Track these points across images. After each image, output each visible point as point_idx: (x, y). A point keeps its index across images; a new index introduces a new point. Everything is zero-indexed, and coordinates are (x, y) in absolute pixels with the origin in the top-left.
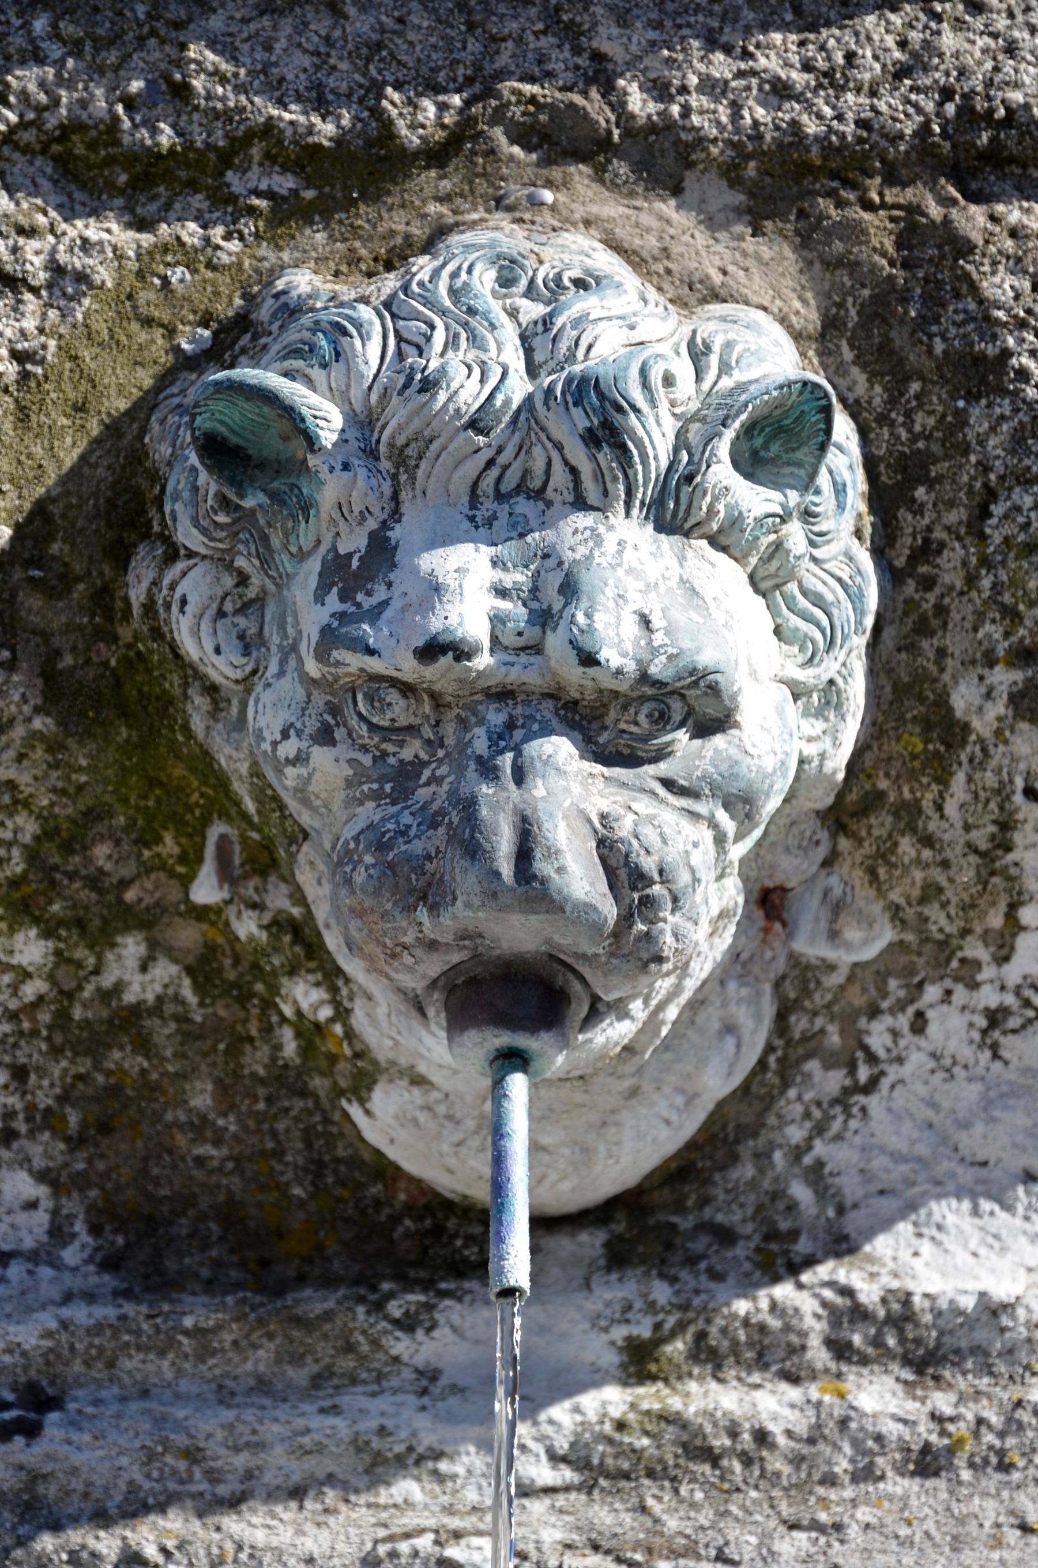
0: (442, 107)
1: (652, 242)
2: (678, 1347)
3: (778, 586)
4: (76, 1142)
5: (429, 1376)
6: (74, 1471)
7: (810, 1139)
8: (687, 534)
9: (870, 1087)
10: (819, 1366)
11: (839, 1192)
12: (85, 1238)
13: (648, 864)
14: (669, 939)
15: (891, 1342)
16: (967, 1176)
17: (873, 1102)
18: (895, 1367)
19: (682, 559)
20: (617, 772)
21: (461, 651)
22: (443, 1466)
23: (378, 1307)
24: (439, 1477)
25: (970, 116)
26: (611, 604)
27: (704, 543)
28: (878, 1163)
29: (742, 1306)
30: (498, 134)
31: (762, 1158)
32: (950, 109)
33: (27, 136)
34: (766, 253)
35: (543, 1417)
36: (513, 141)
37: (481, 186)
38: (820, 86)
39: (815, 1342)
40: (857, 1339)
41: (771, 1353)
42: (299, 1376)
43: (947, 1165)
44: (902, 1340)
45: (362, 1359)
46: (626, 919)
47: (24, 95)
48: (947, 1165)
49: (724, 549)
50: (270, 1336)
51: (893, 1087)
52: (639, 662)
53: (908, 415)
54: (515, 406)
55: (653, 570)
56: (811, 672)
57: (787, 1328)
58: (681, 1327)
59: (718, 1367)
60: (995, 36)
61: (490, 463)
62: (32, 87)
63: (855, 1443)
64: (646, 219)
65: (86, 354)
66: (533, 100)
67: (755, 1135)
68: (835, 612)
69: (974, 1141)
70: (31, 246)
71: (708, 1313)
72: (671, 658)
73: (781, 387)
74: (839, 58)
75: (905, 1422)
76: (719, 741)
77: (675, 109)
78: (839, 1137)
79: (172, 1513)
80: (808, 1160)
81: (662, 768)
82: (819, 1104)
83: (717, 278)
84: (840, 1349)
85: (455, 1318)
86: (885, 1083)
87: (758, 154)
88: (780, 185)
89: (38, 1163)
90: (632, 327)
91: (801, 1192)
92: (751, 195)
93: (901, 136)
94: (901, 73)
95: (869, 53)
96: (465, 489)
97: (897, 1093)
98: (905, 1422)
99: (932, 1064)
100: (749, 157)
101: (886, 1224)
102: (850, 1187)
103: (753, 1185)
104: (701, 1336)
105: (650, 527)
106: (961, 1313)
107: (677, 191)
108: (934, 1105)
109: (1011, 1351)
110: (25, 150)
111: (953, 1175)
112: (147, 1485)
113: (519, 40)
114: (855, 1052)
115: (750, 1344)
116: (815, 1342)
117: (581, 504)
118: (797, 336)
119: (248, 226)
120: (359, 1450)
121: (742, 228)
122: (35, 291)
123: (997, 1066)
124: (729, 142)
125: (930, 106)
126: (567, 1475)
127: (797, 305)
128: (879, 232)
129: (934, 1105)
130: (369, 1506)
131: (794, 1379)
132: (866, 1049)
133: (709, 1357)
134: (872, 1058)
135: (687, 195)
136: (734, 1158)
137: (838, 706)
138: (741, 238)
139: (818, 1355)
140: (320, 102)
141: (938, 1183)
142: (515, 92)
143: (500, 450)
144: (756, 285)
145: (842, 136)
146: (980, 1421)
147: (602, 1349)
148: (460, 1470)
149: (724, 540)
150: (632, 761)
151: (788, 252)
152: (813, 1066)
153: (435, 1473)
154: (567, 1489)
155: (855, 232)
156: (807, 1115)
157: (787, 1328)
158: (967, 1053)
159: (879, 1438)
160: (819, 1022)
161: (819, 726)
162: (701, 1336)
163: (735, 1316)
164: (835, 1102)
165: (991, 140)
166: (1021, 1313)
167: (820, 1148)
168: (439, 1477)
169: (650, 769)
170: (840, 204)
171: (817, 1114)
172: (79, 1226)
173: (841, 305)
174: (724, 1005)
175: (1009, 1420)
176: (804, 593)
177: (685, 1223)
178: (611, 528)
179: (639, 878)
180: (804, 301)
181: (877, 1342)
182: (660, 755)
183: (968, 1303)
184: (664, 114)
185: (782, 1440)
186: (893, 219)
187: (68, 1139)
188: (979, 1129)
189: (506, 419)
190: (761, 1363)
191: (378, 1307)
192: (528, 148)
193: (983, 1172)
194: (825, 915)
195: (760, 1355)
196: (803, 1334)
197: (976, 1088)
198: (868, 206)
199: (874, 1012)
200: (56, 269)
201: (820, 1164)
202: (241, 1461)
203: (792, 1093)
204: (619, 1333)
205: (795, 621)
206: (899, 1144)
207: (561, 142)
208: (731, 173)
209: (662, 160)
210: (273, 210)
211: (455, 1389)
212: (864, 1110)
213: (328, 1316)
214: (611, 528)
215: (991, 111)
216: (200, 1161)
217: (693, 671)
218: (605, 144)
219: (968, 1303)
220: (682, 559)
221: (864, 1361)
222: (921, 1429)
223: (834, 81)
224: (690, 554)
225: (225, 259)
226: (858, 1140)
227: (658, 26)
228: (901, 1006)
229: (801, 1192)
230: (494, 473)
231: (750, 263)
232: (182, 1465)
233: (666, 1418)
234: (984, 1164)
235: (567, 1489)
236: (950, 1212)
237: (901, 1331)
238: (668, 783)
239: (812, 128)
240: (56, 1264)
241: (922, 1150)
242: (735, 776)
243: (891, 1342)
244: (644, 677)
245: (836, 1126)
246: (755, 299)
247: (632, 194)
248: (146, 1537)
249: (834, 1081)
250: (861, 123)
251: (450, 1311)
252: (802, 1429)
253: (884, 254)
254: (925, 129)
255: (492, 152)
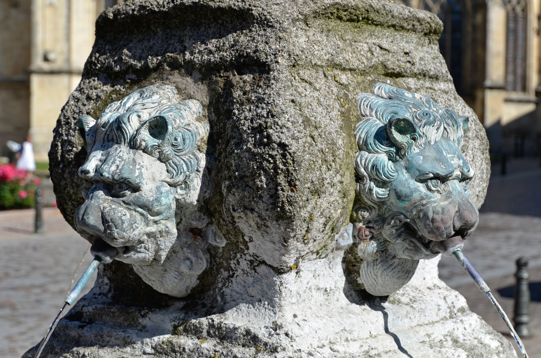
0: (157, 59)
1: (184, 86)
2: (181, 328)
3: (167, 161)
4: (114, 273)
5: (144, 327)
6: (85, 336)
7: (222, 287)
8: (137, 149)
9: (232, 276)
10: (204, 336)
11: (226, 299)
12: (113, 292)
13: (109, 218)
14: (116, 234)
15: (217, 333)
16: (249, 299)
17: (233, 279)
18: (217, 339)
19: (135, 154)
20: (115, 199)
21: (88, 172)
22: (135, 346)
23: (140, 312)
24: (133, 348)
25: (240, 56)
26: (110, 164)
27: (141, 151)
28: (234, 293)
29: (193, 321)
30: (165, 64)
31: (214, 289)
32: (237, 54)
33: (102, 69)
34: (202, 88)
35: (152, 338)
36: (167, 66)
37: (161, 76)
38: (217, 51)
39: (205, 331)
40: (211, 331)
41: (196, 332)
42: (126, 324)
43: (245, 296)
44: (219, 333)
45: (135, 322)
46: (105, 230)
47: (101, 61)
48: (245, 296)
49: (146, 153)
50: (123, 315)
51: (237, 277)
52: (112, 176)
53: (219, 124)
54: (110, 122)
55: (126, 157)
56: (172, 180)
57: (200, 327)
58: (182, 324)
59: (188, 334)
60: (251, 37)
61: (105, 134)
62: (102, 60)
63: (199, 354)
64: (184, 81)
65: (98, 112)
66: (171, 57)
67: (214, 285)
68: (179, 167)
69: (251, 290)
70: (94, 91)
71: (187, 321)
72: (119, 175)
73: (154, 118)
74: (222, 44)
75: (208, 350)
76: (137, 194)
77: (192, 57)
78: (227, 287)
79: (95, 347)
80: (222, 291)
81: (124, 199)
82: (224, 279)
83: (192, 93)
84: (209, 333)
85: (150, 316)
86: (235, 275)
87: (204, 66)
88: (206, 72)
89: (108, 276)
90: (144, 105)
91: (219, 298)
92: (203, 75)
93: (227, 61)
94: (233, 46)
95: (227, 43)
96: (102, 139)
97: (238, 278)
98: (208, 350)
99: (242, 272)
100: (203, 67)
101: (231, 308)
102: (228, 298)
103: (212, 295)
104: (186, 326)
105: (128, 148)
106: (230, 329)
107: (191, 75)
108: (245, 282)
109: (236, 339)
110: (102, 72)
111: (246, 298)
112: (94, 341)
113: (173, 44)
114: (229, 269)
115: (194, 330)
116: (205, 331)
117: (117, 143)
118: (203, 106)
119: (127, 86)
120: (124, 340)
121: (200, 83)
122: (93, 100)
123: (256, 274)
124: (199, 64)
125: (234, 54)
126: (153, 351)
127: (205, 99)
128: (221, 82)
129: (245, 282)
130: (122, 351)
131: (199, 338)
132: (231, 267)
133: (187, 331)
134: (232, 270)
135: (193, 76)
136: (210, 289)
137: (189, 188)
138: (199, 85)
139: (205, 334)
140: (139, 61)
141: (243, 300)
142: (168, 56)
143: (107, 131)
144: (198, 95)
145: (216, 61)
146: (222, 353)
147: (170, 327)
148: (137, 347)
149: (146, 151)
150: (118, 196)
151: (206, 88)
152: (222, 270)
153: (133, 347)
154: (152, 354)
155: (217, 82)
156: (222, 281)
157: (200, 327)
158: (248, 270)
159: (202, 353)
160: (221, 260)
161: (184, 192)
162: (186, 326)
163: (191, 323)
164: (227, 279)
165: (243, 61)
166: (239, 330)
167: (224, 289)
168: (133, 348)
169: (121, 199)
170: (216, 77)
171: (224, 281)
172: (112, 290)
173: (212, 99)
174: (184, 253)
175: (227, 354)
176: (173, 162)
177: (200, 302)
178: (120, 148)
179: (107, 222)
180: (206, 98)
181: (214, 333)
182: (124, 196)
183: (231, 327)
184: (191, 59)
185: (187, 350)
186: (224, 79)
187: (113, 272)
188: (251, 288)
189: (108, 125)
190: (195, 334)
191: (140, 312)
192: (169, 67)
193: (252, 298)
194: (213, 236)
195: (196, 332)
196: (203, 329)
197: (252, 278)
198: (221, 77)
199: (231, 259)
200: (97, 95)
201: (224, 292)
202: (108, 339)
203: (219, 276)
204: (173, 323)
205: (171, 168)
206: (238, 290)
207: (175, 65)
208: (200, 70)
209: (189, 68)
210: (131, 82)
211: (147, 331)
212: (232, 281)
213: (132, 312)
214: (120, 148)
215: (243, 54)
216: (130, 278)
217: (122, 178)
218: (181, 66)
219: (231, 327)
220: (135, 154)
221: (212, 337)
222: (211, 353)
223: (219, 49)
224: (137, 153)
225: (122, 92)
226: (230, 288)
227: (195, 39)
228: (234, 259)
229: (219, 298)
230: (106, 136)
231: (199, 90)
232: (100, 338)
233: (171, 342)
234: (253, 296)
235: (152, 354)
236: (243, 306)
237: (219, 331)
238: (124, 202)
239: (213, 60)
240: (106, 297)
241: (242, 292)
242: (139, 201)
243: (217, 333)
244: (113, 179)
245: (227, 284)
246: (197, 98)
247: (183, 76)
248: (87, 351)
249: (226, 274)
250: (221, 58)
251: (150, 315)
252: (191, 349)
253: (220, 87)
254: (231, 60)
255: (163, 68)
